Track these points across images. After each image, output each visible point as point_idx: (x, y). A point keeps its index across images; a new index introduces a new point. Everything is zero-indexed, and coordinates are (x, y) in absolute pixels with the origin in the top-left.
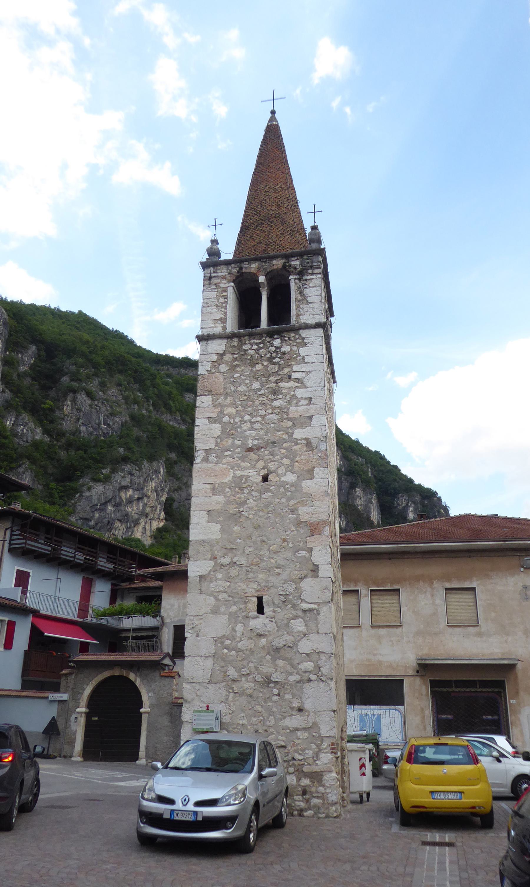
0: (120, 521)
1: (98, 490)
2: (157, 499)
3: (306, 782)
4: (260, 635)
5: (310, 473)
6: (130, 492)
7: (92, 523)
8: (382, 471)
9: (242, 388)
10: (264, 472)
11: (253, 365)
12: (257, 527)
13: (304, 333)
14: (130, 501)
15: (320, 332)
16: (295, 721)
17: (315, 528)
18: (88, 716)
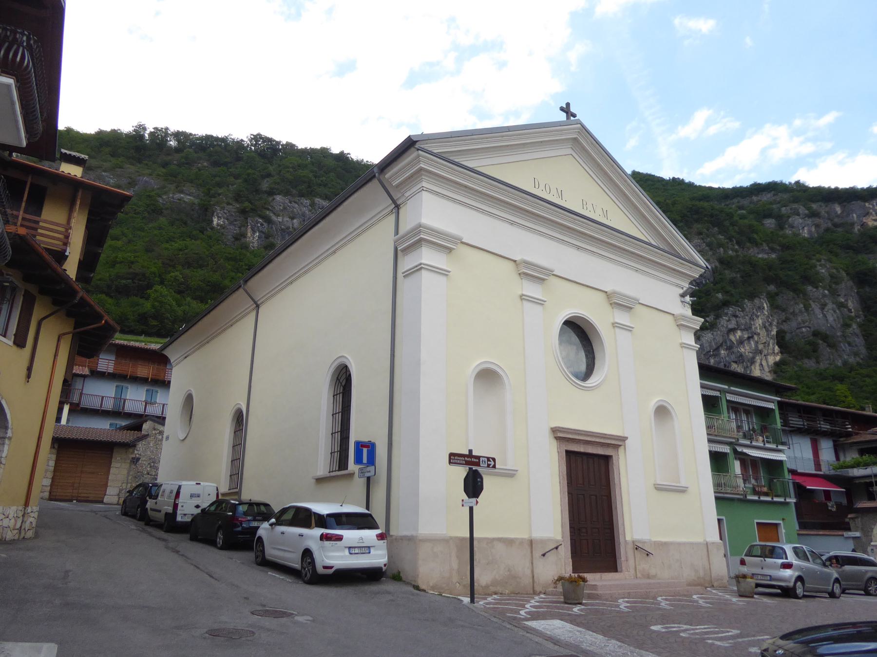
0: (736, 362)
2: (768, 335)
6: (739, 333)
14: (741, 342)
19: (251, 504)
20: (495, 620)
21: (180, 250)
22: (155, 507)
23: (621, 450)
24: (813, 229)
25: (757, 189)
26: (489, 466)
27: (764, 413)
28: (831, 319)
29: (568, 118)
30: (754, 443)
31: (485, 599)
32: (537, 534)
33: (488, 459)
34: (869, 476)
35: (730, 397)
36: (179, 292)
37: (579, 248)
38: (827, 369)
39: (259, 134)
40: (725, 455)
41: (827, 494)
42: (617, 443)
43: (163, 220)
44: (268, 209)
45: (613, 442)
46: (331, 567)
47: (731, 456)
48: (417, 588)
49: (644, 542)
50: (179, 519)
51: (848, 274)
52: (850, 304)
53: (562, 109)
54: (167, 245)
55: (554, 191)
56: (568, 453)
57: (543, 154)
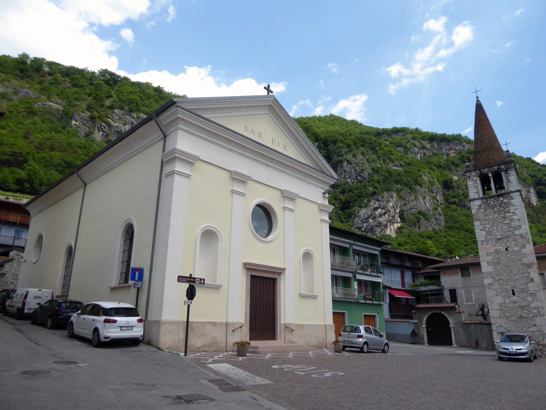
0: (377, 226)
1: (363, 212)
2: (395, 212)
3: (541, 347)
4: (515, 302)
5: (524, 246)
6: (380, 210)
7: (363, 229)
8: (534, 170)
9: (491, 217)
10: (506, 247)
11: (494, 208)
12: (507, 266)
13: (512, 194)
14: (380, 215)
15: (518, 193)
16: (534, 329)
17: (530, 266)
18: (427, 328)
19: (71, 302)
20: (192, 364)
21: (48, 139)
22: (12, 304)
23: (282, 275)
24: (422, 155)
25: (396, 131)
26: (200, 283)
27: (373, 257)
29: (268, 93)
30: (365, 272)
31: (213, 357)
32: (230, 320)
33: (201, 279)
34: (427, 291)
35: (354, 247)
36: (46, 166)
37: (267, 165)
38: (424, 232)
39: (106, 70)
40: (349, 278)
41: (407, 299)
42: (280, 271)
43: (37, 119)
44: (109, 118)
45: (278, 271)
46: (109, 338)
47: (353, 280)
48: (159, 349)
49: (291, 324)
50: (26, 311)
51: (438, 181)
52: (438, 198)
53: (265, 88)
54: (38, 135)
55: (256, 133)
56: (252, 276)
57: (256, 113)
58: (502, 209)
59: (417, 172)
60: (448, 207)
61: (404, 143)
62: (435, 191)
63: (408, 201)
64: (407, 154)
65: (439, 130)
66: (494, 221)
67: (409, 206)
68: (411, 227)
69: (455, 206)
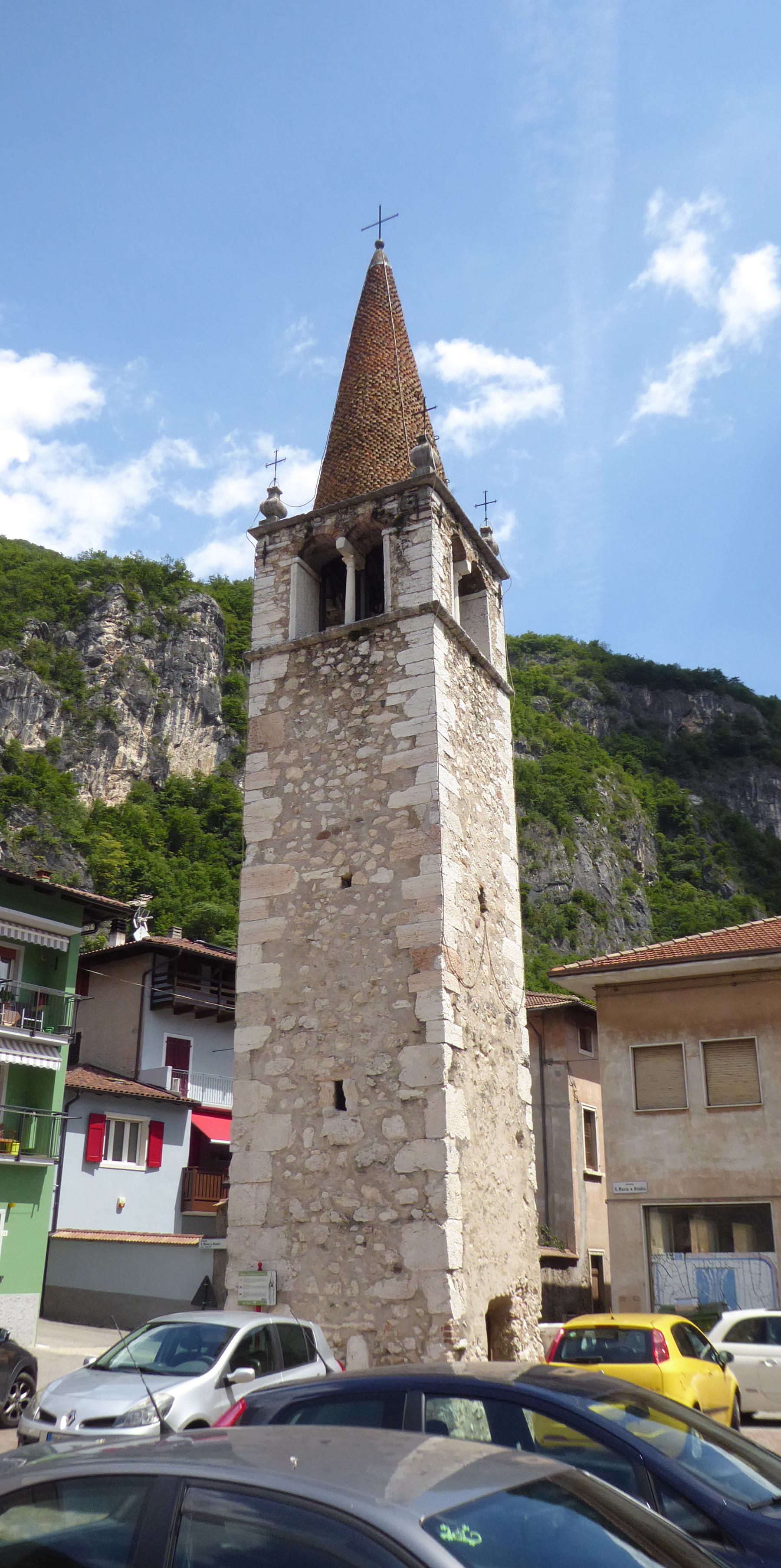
4: (339, 1147)
10: (344, 871)
11: (328, 692)
12: (334, 964)
24: (606, 724)
28: (605, 874)
51: (644, 806)
52: (640, 857)
58: (358, 693)
59: (582, 773)
60: (669, 887)
61: (553, 684)
62: (631, 834)
63: (545, 859)
64: (559, 716)
65: (660, 654)
66: (323, 750)
67: (545, 875)
68: (546, 940)
69: (687, 884)
